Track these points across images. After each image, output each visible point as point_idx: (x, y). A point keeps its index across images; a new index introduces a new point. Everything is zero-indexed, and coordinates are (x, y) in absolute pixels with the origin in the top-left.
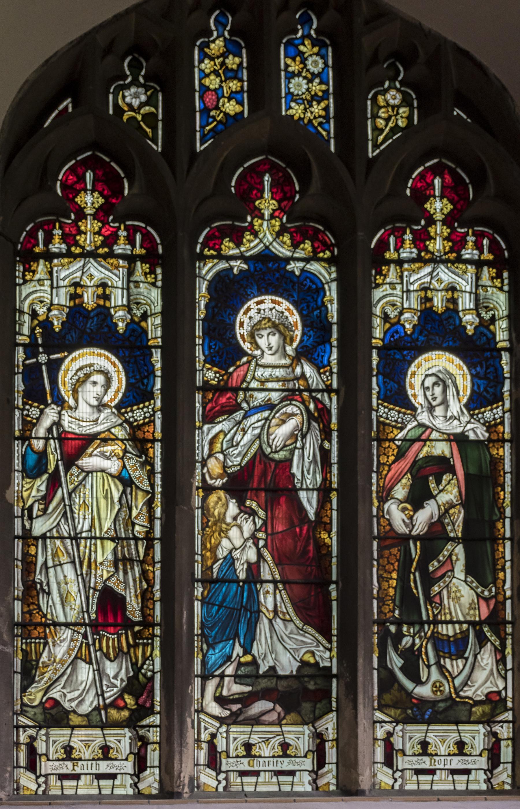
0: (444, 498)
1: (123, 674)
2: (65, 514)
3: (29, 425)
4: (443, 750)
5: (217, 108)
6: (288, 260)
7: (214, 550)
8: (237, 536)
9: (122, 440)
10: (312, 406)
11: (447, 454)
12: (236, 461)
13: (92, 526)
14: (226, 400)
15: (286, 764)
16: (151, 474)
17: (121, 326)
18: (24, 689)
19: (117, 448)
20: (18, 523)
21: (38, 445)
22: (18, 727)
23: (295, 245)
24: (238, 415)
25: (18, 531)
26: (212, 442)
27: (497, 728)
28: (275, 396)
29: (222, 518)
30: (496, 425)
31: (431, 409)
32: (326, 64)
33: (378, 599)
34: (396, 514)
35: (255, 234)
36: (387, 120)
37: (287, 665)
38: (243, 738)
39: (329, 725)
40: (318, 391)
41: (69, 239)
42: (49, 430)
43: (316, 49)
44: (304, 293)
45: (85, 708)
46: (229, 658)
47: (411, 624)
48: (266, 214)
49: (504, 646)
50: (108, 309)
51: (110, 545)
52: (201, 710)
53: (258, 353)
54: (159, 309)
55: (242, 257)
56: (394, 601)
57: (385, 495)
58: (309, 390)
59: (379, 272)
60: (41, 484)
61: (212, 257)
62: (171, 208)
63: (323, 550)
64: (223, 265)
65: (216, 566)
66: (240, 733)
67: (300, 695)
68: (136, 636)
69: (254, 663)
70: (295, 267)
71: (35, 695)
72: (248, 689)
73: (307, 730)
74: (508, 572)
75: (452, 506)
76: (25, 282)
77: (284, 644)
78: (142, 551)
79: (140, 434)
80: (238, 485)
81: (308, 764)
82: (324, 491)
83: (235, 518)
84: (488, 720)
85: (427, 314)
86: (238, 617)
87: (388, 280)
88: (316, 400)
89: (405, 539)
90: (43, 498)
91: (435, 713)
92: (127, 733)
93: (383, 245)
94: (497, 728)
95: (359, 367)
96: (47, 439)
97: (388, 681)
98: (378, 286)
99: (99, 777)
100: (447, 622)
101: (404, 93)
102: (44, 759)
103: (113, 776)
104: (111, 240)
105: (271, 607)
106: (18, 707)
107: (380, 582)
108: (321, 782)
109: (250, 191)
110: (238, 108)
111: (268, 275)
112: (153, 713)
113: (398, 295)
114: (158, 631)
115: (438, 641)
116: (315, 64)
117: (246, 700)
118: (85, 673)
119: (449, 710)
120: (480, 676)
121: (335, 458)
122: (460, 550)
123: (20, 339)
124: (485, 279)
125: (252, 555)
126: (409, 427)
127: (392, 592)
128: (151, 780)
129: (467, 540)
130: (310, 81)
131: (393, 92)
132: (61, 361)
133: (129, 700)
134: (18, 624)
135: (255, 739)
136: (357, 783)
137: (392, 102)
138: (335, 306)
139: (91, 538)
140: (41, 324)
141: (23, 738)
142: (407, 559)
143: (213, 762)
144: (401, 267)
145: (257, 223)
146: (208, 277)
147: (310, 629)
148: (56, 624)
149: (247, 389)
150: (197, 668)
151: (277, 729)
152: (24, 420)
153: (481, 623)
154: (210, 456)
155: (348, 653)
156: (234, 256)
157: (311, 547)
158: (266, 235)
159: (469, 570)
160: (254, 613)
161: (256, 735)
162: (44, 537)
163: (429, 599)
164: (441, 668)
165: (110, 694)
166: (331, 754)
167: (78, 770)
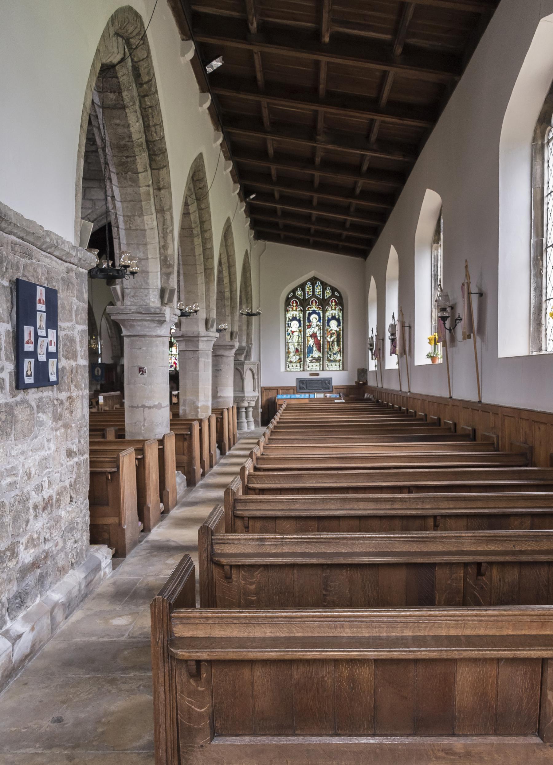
8: (311, 342)
14: (309, 327)
44: (318, 314)
62: (304, 303)
67: (318, 360)
77: (316, 354)
86: (311, 351)
95: (325, 322)
111: (314, 312)
113: (329, 314)
119: (335, 361)
158: (314, 308)
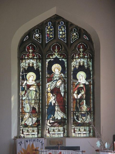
0: (82, 93)
1: (36, 120)
2: (27, 96)
3: (22, 83)
4: (82, 130)
5: (49, 36)
6: (59, 58)
7: (49, 101)
8: (52, 99)
9: (36, 86)
10: (63, 80)
11: (83, 87)
12: (52, 88)
13: (31, 98)
14: (50, 79)
15: (59, 133)
16: (40, 90)
17: (35, 69)
18: (21, 122)
19: (35, 87)
20: (21, 98)
21: (24, 86)
22: (72, 126)
23: (60, 56)
24: (52, 81)
25: (21, 99)
26: (48, 85)
27: (90, 127)
28: (58, 79)
29: (50, 97)
30: (90, 82)
31: (80, 80)
32: (65, 29)
33: (73, 108)
34: (75, 96)
35: (55, 55)
36: (74, 37)
37: (59, 118)
38: (53, 129)
39: (65, 127)
40: (64, 78)
41: (28, 56)
42: (25, 84)
43: (63, 27)
44: (62, 63)
45: (30, 125)
46: (51, 117)
47: (77, 112)
48: (56, 52)
49: (91, 115)
50: (34, 66)
51: (34, 101)
52: (47, 125)
53: (55, 72)
54: (41, 66)
55: (53, 58)
56: (75, 108)
57: (74, 93)
58: (62, 77)
59: (73, 60)
60: (24, 92)
61: (48, 59)
63: (64, 101)
64: (50, 60)
65: (49, 104)
66: (53, 128)
67: (61, 122)
68: (38, 114)
69: (55, 118)
70: (60, 60)
71: (23, 123)
72: (54, 121)
73: (62, 127)
74: (92, 104)
75: (83, 94)
76: (22, 63)
77: (59, 115)
78: (38, 101)
79: (38, 84)
80: (52, 92)
81: (62, 133)
82: (65, 92)
83: (52, 97)
84: (89, 126)
85: (80, 66)
86: (52, 110)
87: (74, 61)
88: (63, 79)
89: (77, 99)
90: (24, 94)
91: (81, 125)
92: (36, 128)
93: (73, 56)
94: (90, 127)
96: (25, 86)
97: (74, 120)
98: (73, 62)
99: (32, 135)
100: (83, 111)
101: (76, 33)
102: (24, 132)
103: (34, 135)
104: (34, 56)
105: (57, 110)
106: (21, 125)
107: (72, 105)
108: (64, 135)
109: (54, 49)
110: (52, 36)
111: (56, 61)
112: (40, 125)
113: (75, 63)
114: (41, 113)
115: (81, 114)
116: (63, 30)
117: (53, 123)
118: (30, 119)
119: (83, 124)
120: (88, 119)
121: (66, 88)
122: (85, 101)
123: (21, 71)
124: (88, 60)
125: (54, 102)
126: (77, 83)
127: (75, 107)
128: (40, 135)
129: (86, 99)
130: (63, 32)
131: (75, 33)
132: (27, 74)
133: (37, 123)
134: (21, 112)
135: (55, 129)
136: (69, 135)
137: (75, 35)
138: (66, 65)
139: (31, 100)
140: (24, 69)
141: (21, 129)
142: (77, 102)
143: (49, 132)
144: (76, 59)
145: (55, 53)
146: (48, 61)
147: (62, 113)
148: (26, 112)
149: (53, 78)
150: (46, 119)
151: (58, 127)
152: (21, 83)
153: (88, 111)
154: (48, 88)
155: (68, 117)
156: (52, 58)
157: (63, 101)
158: (56, 55)
159: (86, 104)
160: (55, 110)
161: (55, 128)
162: (24, 100)
163: (80, 108)
164: (82, 118)
165: (34, 123)
166: (66, 131)
167: (29, 134)
